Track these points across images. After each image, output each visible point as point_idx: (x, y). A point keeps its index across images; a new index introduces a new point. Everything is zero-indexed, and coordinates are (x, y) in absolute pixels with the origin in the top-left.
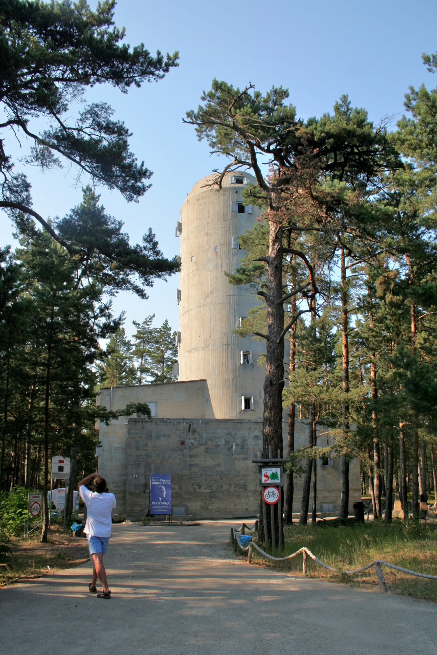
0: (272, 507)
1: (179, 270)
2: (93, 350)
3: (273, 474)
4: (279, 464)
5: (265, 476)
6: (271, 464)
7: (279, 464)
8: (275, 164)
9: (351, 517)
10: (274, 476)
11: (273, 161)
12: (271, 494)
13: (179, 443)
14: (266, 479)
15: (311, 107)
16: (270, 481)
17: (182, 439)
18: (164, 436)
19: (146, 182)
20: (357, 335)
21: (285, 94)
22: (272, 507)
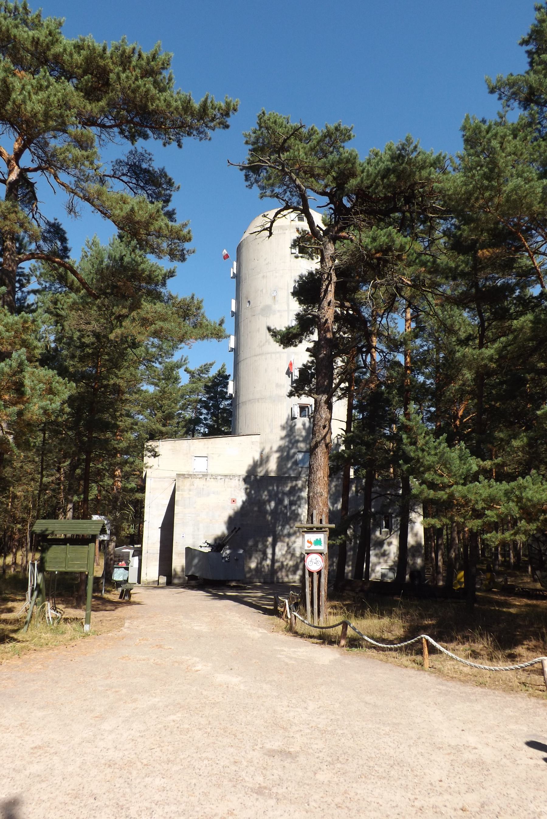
0: (316, 577)
1: (294, 294)
2: (514, 270)
3: (317, 540)
4: (323, 530)
5: (308, 541)
6: (315, 529)
7: (323, 530)
8: (331, 208)
9: (479, 594)
10: (318, 542)
11: (328, 204)
12: (314, 561)
13: (230, 501)
14: (310, 545)
15: (368, 149)
16: (313, 547)
17: (234, 497)
18: (214, 493)
19: (187, 246)
20: (527, 360)
21: (346, 136)
22: (316, 577)
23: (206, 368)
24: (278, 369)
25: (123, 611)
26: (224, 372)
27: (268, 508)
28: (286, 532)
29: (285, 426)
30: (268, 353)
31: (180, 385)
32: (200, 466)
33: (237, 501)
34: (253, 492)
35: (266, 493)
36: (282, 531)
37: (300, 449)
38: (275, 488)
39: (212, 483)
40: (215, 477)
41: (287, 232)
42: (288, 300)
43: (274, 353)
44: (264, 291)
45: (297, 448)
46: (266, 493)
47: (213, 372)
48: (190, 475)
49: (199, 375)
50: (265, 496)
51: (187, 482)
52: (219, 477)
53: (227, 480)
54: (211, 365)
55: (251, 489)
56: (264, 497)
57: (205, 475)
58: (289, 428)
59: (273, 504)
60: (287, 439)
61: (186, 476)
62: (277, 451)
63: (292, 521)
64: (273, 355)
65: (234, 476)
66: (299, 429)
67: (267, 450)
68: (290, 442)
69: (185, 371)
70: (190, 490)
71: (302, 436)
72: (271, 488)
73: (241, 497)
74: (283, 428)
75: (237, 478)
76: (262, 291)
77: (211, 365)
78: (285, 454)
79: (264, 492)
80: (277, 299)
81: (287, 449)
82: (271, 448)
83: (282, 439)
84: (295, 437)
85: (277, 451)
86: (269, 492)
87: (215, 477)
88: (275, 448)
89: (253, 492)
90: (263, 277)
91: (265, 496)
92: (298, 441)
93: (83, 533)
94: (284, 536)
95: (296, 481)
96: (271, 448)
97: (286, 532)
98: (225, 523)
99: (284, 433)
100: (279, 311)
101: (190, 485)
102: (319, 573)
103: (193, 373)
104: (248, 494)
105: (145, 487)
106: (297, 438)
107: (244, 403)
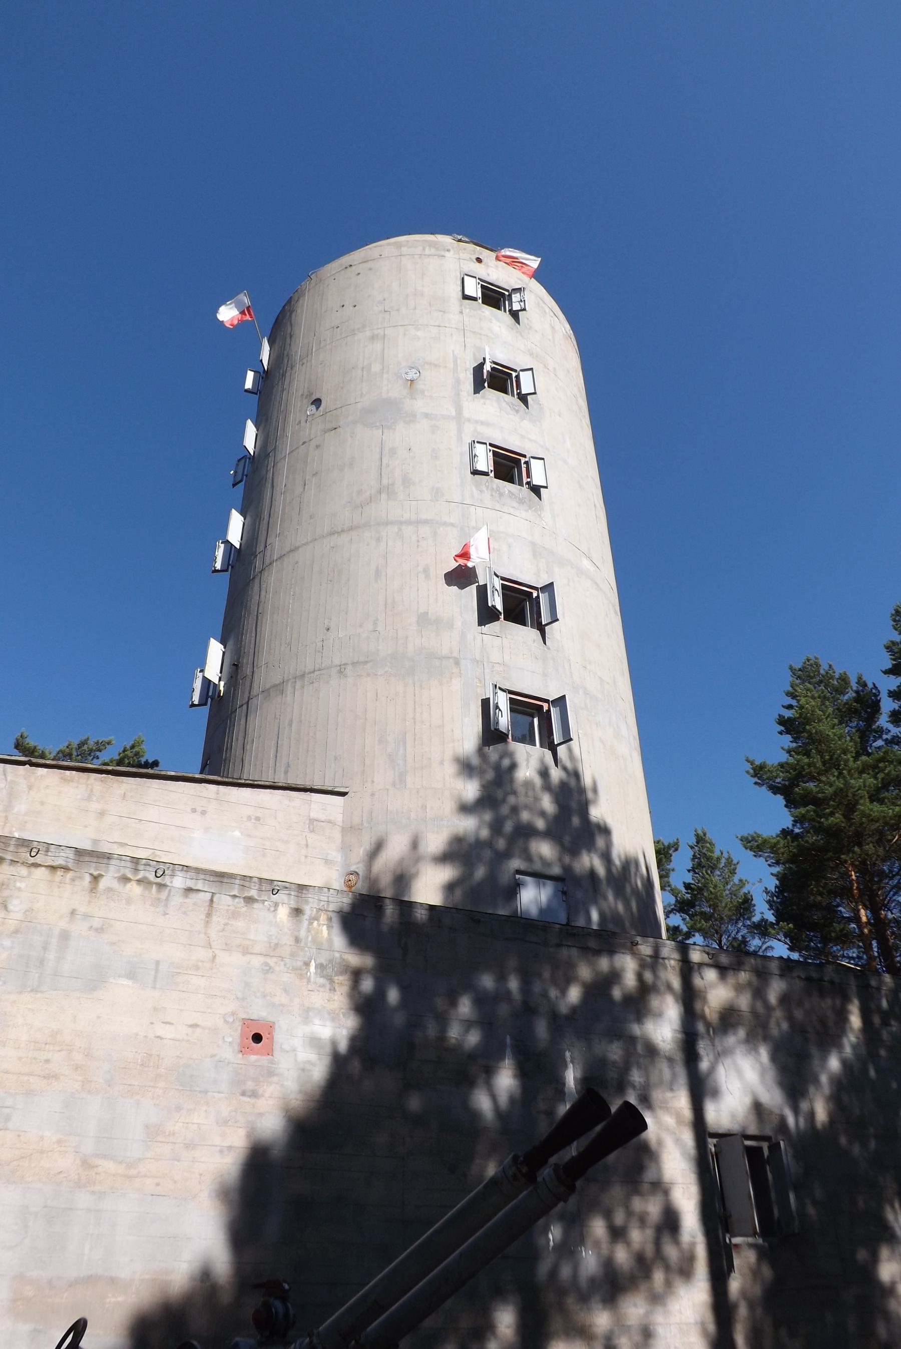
13: (233, 1035)
17: (258, 1011)
18: (131, 975)
25: (276, 1026)
27: (483, 1102)
28: (590, 1261)
29: (475, 761)
33: (281, 1038)
34: (393, 995)
35: (465, 1007)
36: (569, 1249)
37: (538, 867)
38: (513, 984)
41: (447, 254)
42: (458, 395)
43: (409, 522)
44: (376, 368)
45: (527, 856)
46: (465, 1007)
50: (462, 1028)
53: (224, 901)
55: (384, 972)
56: (454, 1032)
57: (89, 857)
58: (490, 775)
59: (506, 1080)
60: (488, 816)
62: (445, 858)
63: (617, 1191)
64: (408, 530)
65: (272, 887)
66: (528, 784)
67: (396, 849)
68: (496, 827)
71: (543, 814)
72: (487, 982)
73: (315, 1026)
74: (466, 768)
78: (480, 872)
79: (453, 1003)
80: (419, 386)
81: (487, 854)
82: (415, 844)
83: (465, 809)
84: (515, 810)
85: (445, 858)
86: (482, 1001)
88: (435, 842)
89: (393, 995)
91: (462, 1028)
92: (526, 832)
94: (584, 1298)
95: (611, 952)
96: (415, 844)
97: (590, 1261)
98: (224, 1194)
99: (471, 790)
100: (426, 415)
104: (367, 1007)
106: (525, 816)
107: (279, 688)
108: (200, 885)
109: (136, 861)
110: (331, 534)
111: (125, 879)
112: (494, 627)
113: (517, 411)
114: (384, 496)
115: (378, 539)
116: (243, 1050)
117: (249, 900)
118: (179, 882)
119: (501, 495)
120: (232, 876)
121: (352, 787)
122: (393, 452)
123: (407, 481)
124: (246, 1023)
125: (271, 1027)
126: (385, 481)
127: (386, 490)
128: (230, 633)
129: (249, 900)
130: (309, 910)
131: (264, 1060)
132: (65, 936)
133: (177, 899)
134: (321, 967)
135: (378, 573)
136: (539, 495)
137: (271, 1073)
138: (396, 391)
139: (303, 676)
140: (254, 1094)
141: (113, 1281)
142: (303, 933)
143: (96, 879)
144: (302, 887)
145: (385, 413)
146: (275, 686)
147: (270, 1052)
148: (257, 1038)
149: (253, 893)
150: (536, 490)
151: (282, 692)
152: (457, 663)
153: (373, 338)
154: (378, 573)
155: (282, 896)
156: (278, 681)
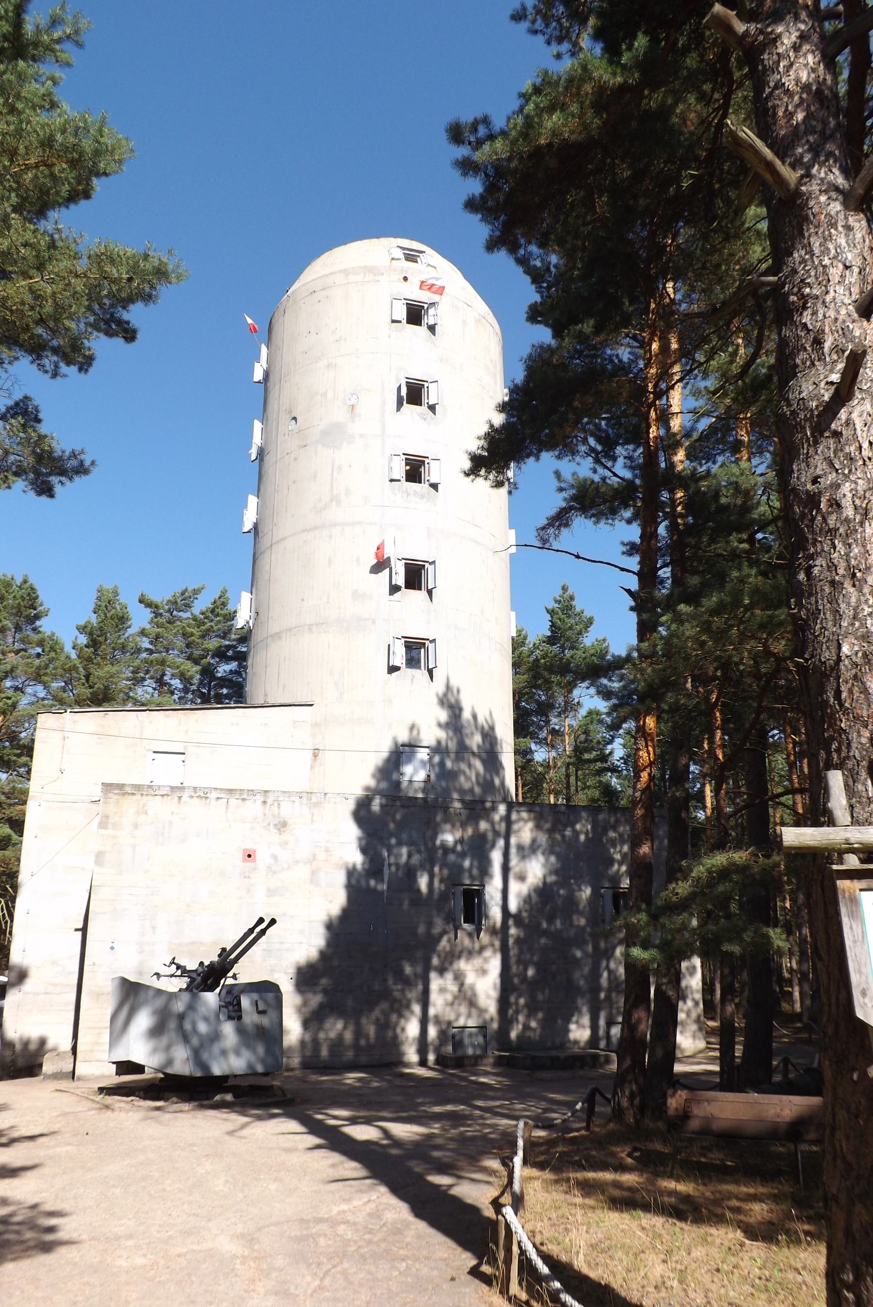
13: (240, 855)
17: (249, 846)
23: (184, 601)
24: (358, 560)
26: (224, 604)
30: (336, 525)
31: (130, 631)
32: (166, 772)
39: (192, 807)
40: (202, 794)
41: (381, 278)
44: (330, 395)
47: (201, 605)
48: (138, 788)
49: (170, 611)
51: (130, 805)
52: (214, 795)
53: (233, 801)
54: (196, 592)
57: (177, 790)
61: (128, 790)
65: (252, 792)
69: (141, 601)
70: (136, 826)
75: (259, 798)
76: (324, 394)
77: (196, 592)
80: (358, 410)
87: (202, 794)
90: (329, 366)
93: (194, 1121)
100: (362, 436)
101: (138, 813)
102: (708, 1043)
103: (157, 607)
105: (23, 822)
107: (278, 636)
108: (222, 796)
109: (195, 788)
110: (304, 531)
111: (192, 797)
112: (398, 595)
113: (425, 419)
114: (334, 503)
115: (331, 537)
116: (244, 861)
117: (244, 800)
118: (214, 795)
119: (408, 495)
120: (236, 790)
121: (317, 701)
122: (340, 468)
123: (348, 492)
124: (245, 850)
125: (254, 851)
126: (335, 492)
127: (335, 499)
128: (253, 585)
129: (244, 800)
130: (269, 801)
131: (252, 864)
132: (171, 823)
133: (213, 802)
134: (275, 825)
135: (330, 562)
136: (437, 490)
137: (255, 869)
138: (339, 415)
139: (290, 630)
140: (249, 877)
141: (201, 943)
142: (267, 812)
143: (180, 798)
144: (266, 792)
145: (334, 435)
146: (277, 634)
147: (254, 861)
148: (249, 856)
149: (245, 796)
150: (435, 486)
151: (280, 638)
152: (374, 622)
153: (329, 366)
154: (330, 562)
155: (258, 797)
156: (277, 631)
